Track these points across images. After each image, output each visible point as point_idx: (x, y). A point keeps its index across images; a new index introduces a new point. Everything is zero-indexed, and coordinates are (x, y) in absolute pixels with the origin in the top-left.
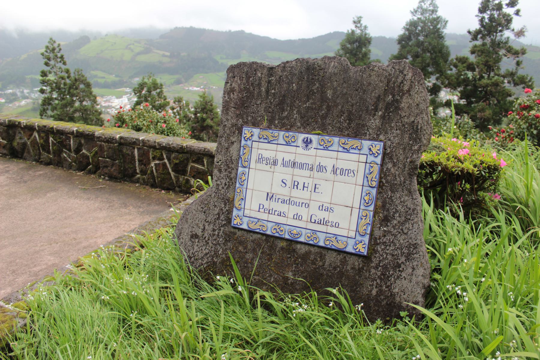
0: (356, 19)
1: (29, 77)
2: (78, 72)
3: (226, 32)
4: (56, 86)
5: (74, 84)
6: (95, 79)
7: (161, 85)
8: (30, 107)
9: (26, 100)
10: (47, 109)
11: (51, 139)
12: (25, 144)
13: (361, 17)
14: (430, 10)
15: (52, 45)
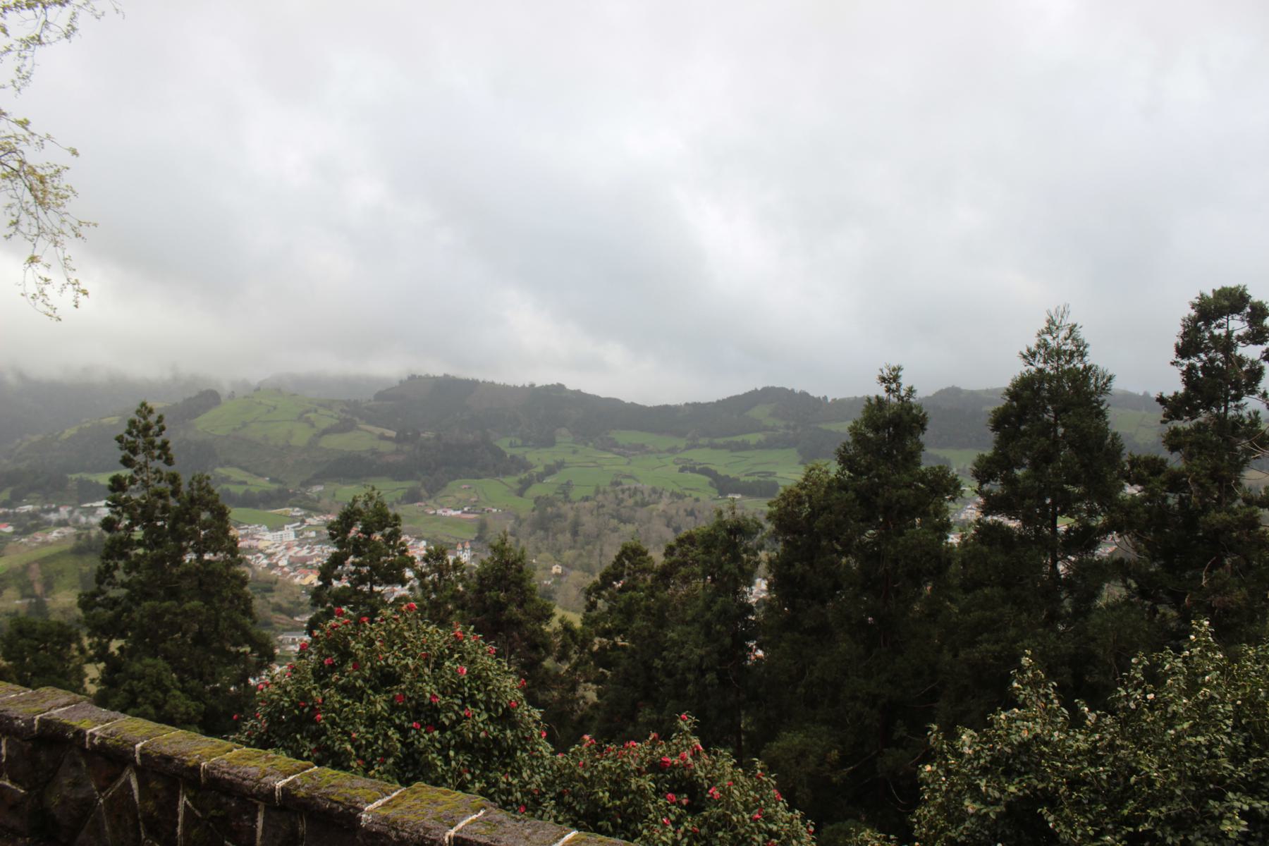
0: (886, 373)
1: (74, 476)
2: (199, 482)
3: (523, 387)
4: (143, 512)
5: (187, 509)
6: (225, 486)
7: (396, 518)
8: (68, 546)
9: (62, 529)
10: (116, 567)
11: (183, 800)
12: (87, 805)
13: (900, 369)
14: (1065, 351)
15: (145, 418)
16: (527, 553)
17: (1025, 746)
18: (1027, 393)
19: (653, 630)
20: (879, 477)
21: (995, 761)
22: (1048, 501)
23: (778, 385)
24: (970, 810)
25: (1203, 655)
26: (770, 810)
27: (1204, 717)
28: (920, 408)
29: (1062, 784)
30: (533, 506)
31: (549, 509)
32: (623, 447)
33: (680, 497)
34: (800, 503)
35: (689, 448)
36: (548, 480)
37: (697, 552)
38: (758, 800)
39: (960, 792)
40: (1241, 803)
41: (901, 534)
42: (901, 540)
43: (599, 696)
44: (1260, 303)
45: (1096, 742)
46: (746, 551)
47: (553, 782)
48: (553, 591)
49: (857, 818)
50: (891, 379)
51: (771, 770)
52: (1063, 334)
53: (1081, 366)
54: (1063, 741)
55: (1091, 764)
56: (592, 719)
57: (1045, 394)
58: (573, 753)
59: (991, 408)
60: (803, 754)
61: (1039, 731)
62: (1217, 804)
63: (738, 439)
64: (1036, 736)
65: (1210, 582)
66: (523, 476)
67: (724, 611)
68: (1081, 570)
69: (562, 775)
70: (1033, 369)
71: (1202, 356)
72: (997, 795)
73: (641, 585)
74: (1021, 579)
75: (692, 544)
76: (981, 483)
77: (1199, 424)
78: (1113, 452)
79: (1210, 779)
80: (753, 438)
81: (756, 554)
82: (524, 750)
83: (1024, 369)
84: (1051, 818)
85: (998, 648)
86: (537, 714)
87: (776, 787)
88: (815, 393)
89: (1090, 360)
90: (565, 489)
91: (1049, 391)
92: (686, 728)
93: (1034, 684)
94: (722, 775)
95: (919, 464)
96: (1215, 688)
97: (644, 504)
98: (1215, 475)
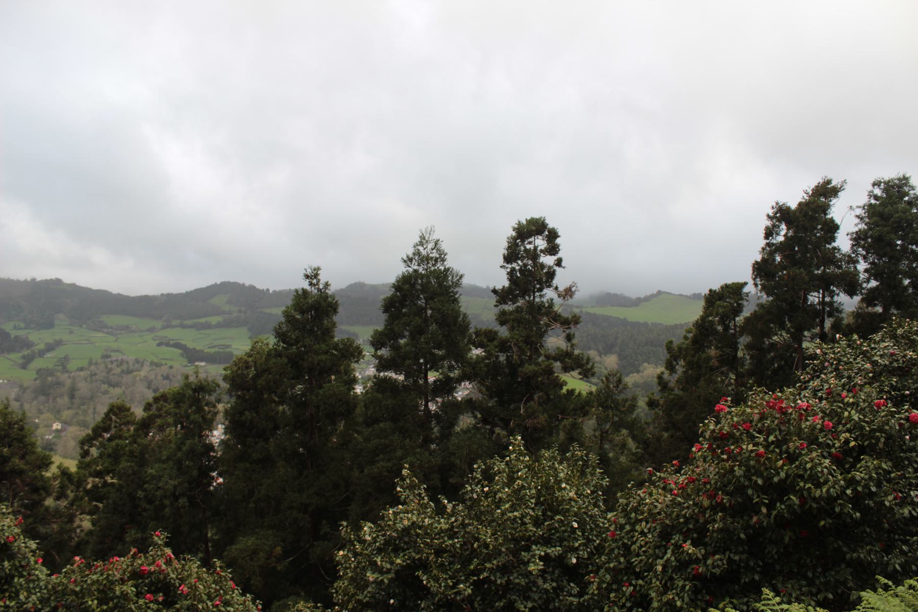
0: (309, 272)
3: (26, 281)
13: (319, 269)
16: (29, 415)
17: (406, 530)
18: (406, 287)
19: (136, 469)
20: (305, 346)
21: (387, 543)
22: (422, 361)
23: (232, 280)
24: (371, 579)
25: (518, 460)
26: (228, 597)
27: (518, 499)
28: (333, 296)
29: (431, 554)
30: (35, 376)
31: (50, 379)
32: (111, 328)
33: (158, 365)
34: (248, 368)
35: (164, 328)
36: (48, 355)
37: (169, 406)
38: (219, 591)
39: (364, 567)
40: (538, 550)
41: (321, 387)
42: (321, 392)
43: (93, 524)
44: (553, 229)
45: (452, 523)
46: (207, 405)
47: (49, 599)
48: (54, 444)
49: (298, 595)
50: (313, 276)
51: (228, 566)
52: (430, 246)
53: (442, 268)
54: (432, 524)
55: (450, 538)
56: (87, 542)
57: (419, 287)
58: (66, 572)
59: (383, 297)
60: (255, 552)
61: (415, 519)
62: (526, 554)
63: (203, 320)
64: (413, 523)
65: (526, 411)
66: (26, 352)
67: (192, 450)
68: (444, 407)
69: (56, 592)
70: (411, 270)
71: (519, 262)
72: (388, 566)
73: (126, 435)
74: (405, 416)
75: (166, 401)
76: (376, 350)
77: (518, 307)
78: (465, 326)
79: (523, 538)
80: (214, 320)
81: (215, 406)
82: (21, 576)
83: (404, 270)
84: (425, 578)
85: (390, 464)
86: (33, 545)
87: (232, 579)
88: (261, 286)
89: (449, 263)
90: (63, 363)
91: (421, 285)
92: (160, 542)
93: (412, 487)
94: (190, 575)
95: (333, 337)
96: (524, 480)
97: (129, 372)
98: (528, 341)
